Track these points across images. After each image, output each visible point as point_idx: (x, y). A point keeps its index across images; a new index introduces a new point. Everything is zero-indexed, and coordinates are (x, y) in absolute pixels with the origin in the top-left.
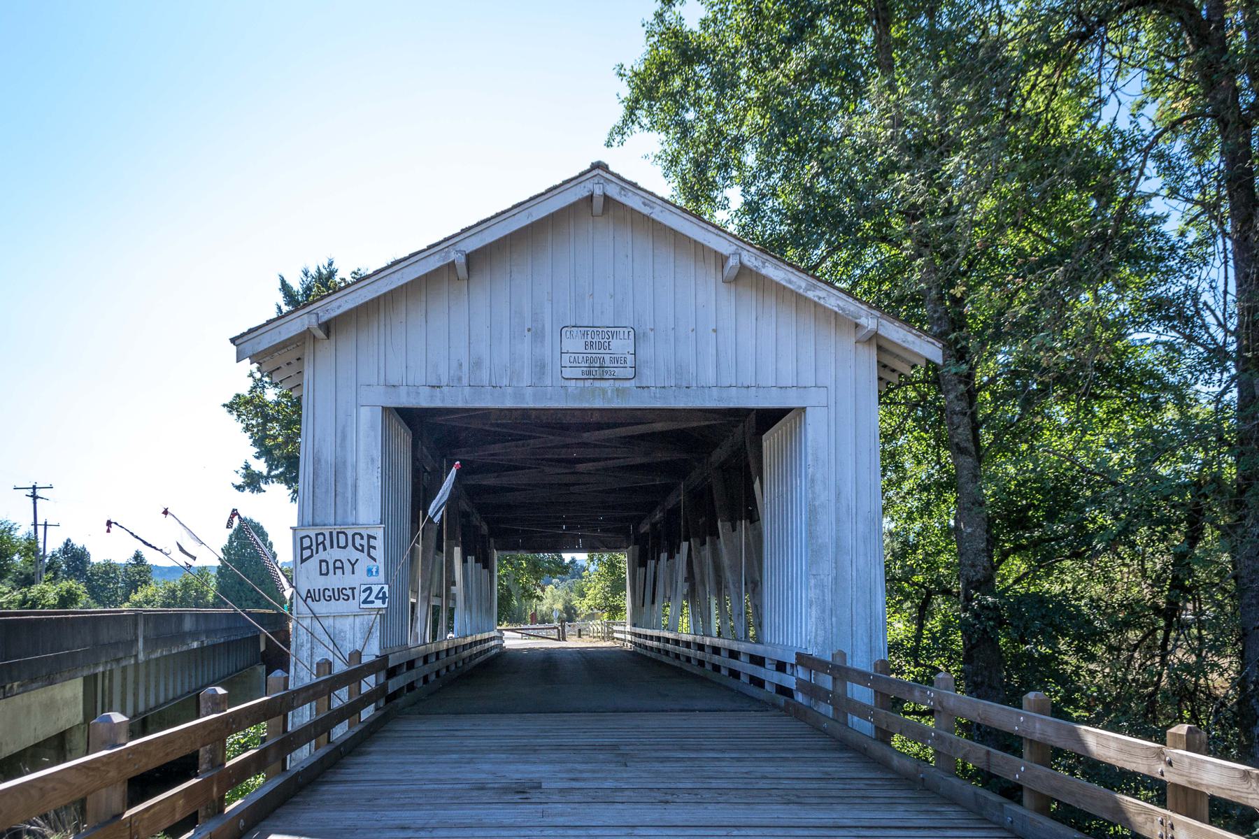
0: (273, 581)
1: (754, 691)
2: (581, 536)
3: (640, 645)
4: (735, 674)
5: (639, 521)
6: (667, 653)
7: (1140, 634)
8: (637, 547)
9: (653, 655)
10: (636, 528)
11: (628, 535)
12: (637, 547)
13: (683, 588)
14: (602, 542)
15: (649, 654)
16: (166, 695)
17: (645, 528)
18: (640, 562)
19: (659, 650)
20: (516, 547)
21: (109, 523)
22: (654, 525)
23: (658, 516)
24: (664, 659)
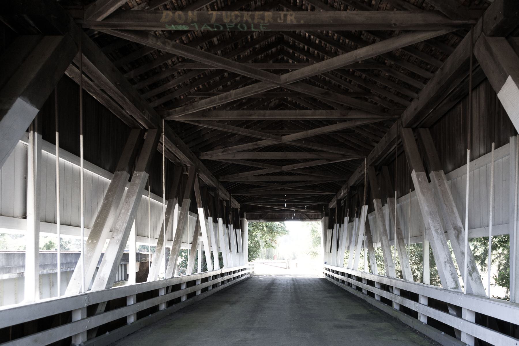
0: (94, 214)
1: (384, 307)
2: (296, 212)
3: (329, 276)
4: (371, 294)
5: (329, 199)
6: (350, 285)
7: (178, 263)
8: (327, 218)
9: (339, 284)
10: (327, 206)
11: (322, 211)
12: (327, 218)
13: (362, 237)
14: (307, 215)
15: (336, 282)
16: (118, 279)
17: (333, 204)
18: (329, 226)
19: (343, 282)
20: (258, 218)
21: (289, 268)
22: (339, 202)
23: (343, 193)
24: (348, 288)
